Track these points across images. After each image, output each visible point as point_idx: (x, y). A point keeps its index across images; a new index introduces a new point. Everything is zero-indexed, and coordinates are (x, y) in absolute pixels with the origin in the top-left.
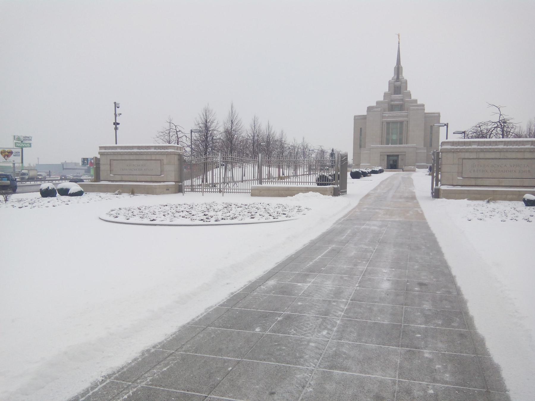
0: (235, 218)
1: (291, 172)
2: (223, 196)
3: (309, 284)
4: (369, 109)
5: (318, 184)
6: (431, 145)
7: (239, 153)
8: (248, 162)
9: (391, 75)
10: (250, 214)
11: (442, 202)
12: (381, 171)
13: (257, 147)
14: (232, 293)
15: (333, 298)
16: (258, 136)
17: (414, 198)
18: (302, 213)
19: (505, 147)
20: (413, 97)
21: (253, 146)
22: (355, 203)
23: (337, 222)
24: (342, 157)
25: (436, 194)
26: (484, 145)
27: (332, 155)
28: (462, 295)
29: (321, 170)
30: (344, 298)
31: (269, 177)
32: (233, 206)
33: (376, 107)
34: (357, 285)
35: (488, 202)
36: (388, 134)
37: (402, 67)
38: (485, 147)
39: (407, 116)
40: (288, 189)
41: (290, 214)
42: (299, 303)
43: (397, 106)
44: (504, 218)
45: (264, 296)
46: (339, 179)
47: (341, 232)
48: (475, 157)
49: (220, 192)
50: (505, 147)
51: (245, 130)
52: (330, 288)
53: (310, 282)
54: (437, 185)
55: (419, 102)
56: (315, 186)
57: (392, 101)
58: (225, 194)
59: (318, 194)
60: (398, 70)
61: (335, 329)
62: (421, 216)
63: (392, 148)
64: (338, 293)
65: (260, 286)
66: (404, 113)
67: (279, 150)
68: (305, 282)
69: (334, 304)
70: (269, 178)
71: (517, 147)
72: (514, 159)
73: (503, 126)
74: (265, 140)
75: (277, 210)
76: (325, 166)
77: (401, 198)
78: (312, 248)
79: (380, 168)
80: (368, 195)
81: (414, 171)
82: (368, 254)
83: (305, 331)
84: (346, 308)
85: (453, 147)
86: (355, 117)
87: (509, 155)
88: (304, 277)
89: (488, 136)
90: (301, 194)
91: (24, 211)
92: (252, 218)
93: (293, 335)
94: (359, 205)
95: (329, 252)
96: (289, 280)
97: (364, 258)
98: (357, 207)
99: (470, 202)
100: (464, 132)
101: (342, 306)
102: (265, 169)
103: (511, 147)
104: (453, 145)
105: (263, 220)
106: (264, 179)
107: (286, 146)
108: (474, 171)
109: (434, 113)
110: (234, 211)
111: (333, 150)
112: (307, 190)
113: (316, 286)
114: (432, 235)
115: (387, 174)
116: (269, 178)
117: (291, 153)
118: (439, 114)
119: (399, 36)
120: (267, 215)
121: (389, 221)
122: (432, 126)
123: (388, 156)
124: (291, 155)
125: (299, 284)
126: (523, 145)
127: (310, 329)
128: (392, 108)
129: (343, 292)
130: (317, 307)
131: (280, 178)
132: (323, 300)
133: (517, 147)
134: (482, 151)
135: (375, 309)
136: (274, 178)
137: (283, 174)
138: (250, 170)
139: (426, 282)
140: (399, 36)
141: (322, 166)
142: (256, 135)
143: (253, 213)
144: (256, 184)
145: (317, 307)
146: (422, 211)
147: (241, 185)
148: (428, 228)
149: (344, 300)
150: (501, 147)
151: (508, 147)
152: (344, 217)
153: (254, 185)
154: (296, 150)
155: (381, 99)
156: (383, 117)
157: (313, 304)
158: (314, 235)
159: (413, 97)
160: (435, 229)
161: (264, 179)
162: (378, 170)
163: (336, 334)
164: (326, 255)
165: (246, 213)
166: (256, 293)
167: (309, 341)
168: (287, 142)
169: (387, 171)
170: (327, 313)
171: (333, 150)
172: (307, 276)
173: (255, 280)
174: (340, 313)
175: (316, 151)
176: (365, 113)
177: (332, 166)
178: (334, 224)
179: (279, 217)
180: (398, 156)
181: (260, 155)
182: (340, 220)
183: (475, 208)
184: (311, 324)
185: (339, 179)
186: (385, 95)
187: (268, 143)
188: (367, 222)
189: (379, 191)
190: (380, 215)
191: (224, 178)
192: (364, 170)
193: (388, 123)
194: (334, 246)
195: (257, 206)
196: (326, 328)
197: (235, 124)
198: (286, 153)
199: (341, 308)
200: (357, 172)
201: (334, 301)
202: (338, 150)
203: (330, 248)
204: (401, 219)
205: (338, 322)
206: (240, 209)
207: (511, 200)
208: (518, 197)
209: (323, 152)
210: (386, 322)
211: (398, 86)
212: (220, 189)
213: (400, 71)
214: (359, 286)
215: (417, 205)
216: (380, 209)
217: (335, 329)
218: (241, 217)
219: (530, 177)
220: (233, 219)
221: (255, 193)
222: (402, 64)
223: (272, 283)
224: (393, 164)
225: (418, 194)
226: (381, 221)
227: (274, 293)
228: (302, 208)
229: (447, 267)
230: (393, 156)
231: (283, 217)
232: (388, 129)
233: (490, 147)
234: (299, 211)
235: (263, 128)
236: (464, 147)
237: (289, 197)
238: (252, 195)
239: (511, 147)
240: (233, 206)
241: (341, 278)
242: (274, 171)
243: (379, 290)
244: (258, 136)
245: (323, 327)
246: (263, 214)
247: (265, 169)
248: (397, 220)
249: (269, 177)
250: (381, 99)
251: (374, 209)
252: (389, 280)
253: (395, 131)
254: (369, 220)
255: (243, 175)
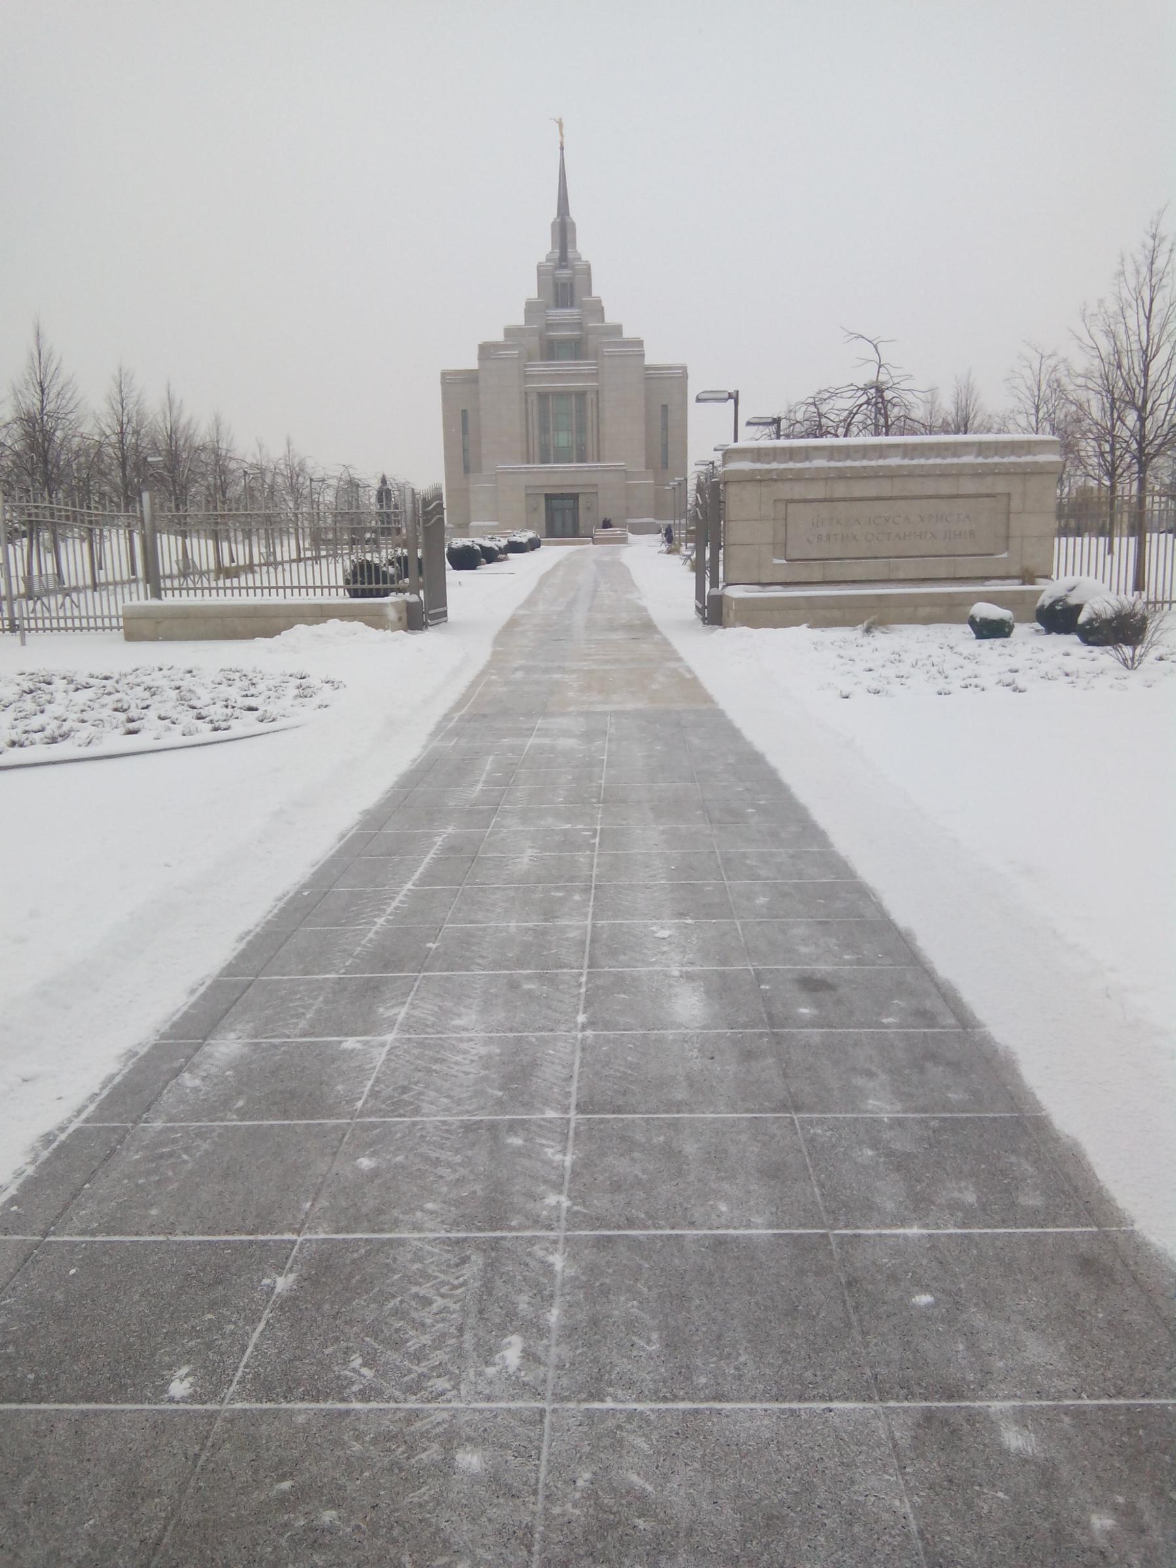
0: (65, 736)
1: (259, 551)
2: (23, 643)
3: (390, 1037)
4: (486, 351)
5: (354, 594)
6: (665, 465)
7: (69, 493)
8: (111, 521)
9: (543, 247)
10: (122, 716)
11: (735, 639)
12: (533, 545)
13: (136, 468)
14: (48, 1139)
15: (500, 1104)
16: (136, 432)
17: (648, 627)
18: (316, 700)
19: (906, 462)
20: (610, 318)
21: (123, 466)
22: (481, 653)
23: (439, 727)
24: (426, 503)
25: (714, 613)
26: (848, 457)
27: (384, 494)
28: (979, 1025)
29: (353, 542)
30: (546, 1102)
31: (187, 569)
32: (60, 684)
33: (504, 346)
34: (581, 1018)
35: (868, 631)
36: (544, 429)
37: (573, 224)
38: (849, 463)
39: (595, 375)
40: (255, 613)
41: (273, 709)
42: (365, 1163)
43: (564, 342)
44: (941, 684)
45: (201, 1134)
46: (421, 572)
47: (463, 768)
48: (821, 496)
49: (13, 628)
50: (906, 462)
51: (90, 414)
52: (483, 1051)
53: (391, 1023)
54: (715, 583)
55: (628, 333)
56: (342, 598)
57: (550, 326)
58: (30, 637)
59: (358, 625)
60: (563, 231)
61: (554, 1316)
62: (691, 686)
63: (562, 474)
64: (517, 1075)
65: (177, 1072)
66: (584, 366)
67: (210, 479)
68: (369, 1025)
69: (516, 1141)
70: (184, 574)
71: (939, 461)
72: (931, 497)
73: (878, 399)
74: (163, 446)
75: (225, 691)
76: (365, 530)
77: (613, 628)
78: (373, 847)
79: (530, 534)
80: (512, 624)
81: (623, 541)
82: (582, 857)
83: (419, 1356)
84: (568, 1160)
85: (759, 466)
86: (444, 374)
87: (916, 487)
88: (360, 1001)
89: (841, 431)
90: (301, 630)
91: (991, 336)
92: (130, 732)
93: (363, 1396)
94: (496, 662)
95: (437, 861)
96: (303, 1024)
97: (572, 879)
98: (490, 665)
99: (817, 632)
100: (777, 421)
101: (551, 1153)
102: (169, 547)
103: (922, 461)
104: (759, 460)
105: (174, 737)
106: (165, 577)
107: (232, 465)
108: (819, 537)
109: (670, 368)
110: (62, 701)
111: (384, 481)
112: (320, 614)
113: (421, 1044)
114: (757, 759)
115: (551, 554)
116: (184, 574)
117: (252, 489)
118: (684, 369)
119: (561, 125)
120: (188, 718)
121: (605, 713)
122: (665, 407)
123: (548, 497)
124: (252, 496)
125: (350, 1043)
126: (954, 455)
127: (439, 1341)
128: (551, 349)
129: (534, 1064)
130: (444, 1171)
131: (223, 572)
132: (468, 1128)
133: (939, 461)
134: (842, 476)
135: (690, 1148)
136: (202, 574)
137: (232, 561)
138: (117, 546)
139: (823, 968)
140: (561, 125)
141: (353, 531)
142: (129, 430)
143: (134, 713)
144: (139, 599)
145: (444, 1171)
146: (689, 670)
147: (91, 603)
148: (734, 734)
149: (551, 1114)
150: (894, 461)
151: (915, 462)
152: (459, 705)
153: (135, 602)
154: (268, 480)
155: (519, 320)
156: (527, 377)
157: (427, 1159)
158: (371, 788)
159: (610, 318)
160: (757, 735)
161: (165, 577)
162: (524, 540)
163: (565, 1351)
164: (429, 877)
165: (106, 713)
166: (158, 1124)
167: (451, 1439)
168: (238, 454)
169: (549, 544)
170: (495, 1209)
171: (384, 481)
172: (371, 991)
173: (153, 1039)
174: (552, 1199)
175: (334, 482)
176: (472, 363)
177: (386, 532)
178: (433, 735)
179: (232, 722)
180: (575, 497)
181: (146, 496)
182: (447, 717)
183: (842, 653)
184: (439, 1302)
185: (421, 572)
186: (531, 309)
187: (173, 456)
188: (540, 723)
189: (541, 608)
190: (571, 694)
191: (28, 580)
192: (487, 543)
193: (543, 396)
194: (450, 830)
195: (148, 681)
196: (510, 1320)
197: (52, 395)
198: (235, 491)
199: (548, 1163)
200: (467, 550)
201: (513, 1127)
202: (401, 480)
203: (439, 840)
204: (640, 705)
205: (558, 1261)
206: (83, 696)
207: (927, 621)
208: (948, 611)
209: (353, 486)
210: (760, 1231)
211: (564, 281)
212: (12, 620)
213: (569, 237)
214: (591, 1024)
215: (669, 653)
216: (561, 669)
217: (554, 1316)
218: (86, 731)
219: (974, 551)
220: (53, 740)
221: (140, 628)
222: (574, 213)
223: (228, 1046)
224: (563, 517)
225: (657, 614)
226: (581, 714)
227: (243, 1114)
228: (314, 681)
229: (863, 892)
230: (562, 496)
231: (245, 724)
232: (544, 413)
233: (865, 463)
234: (304, 692)
235: (152, 406)
236: (791, 465)
237: (261, 642)
238: (130, 637)
239: (922, 461)
240: (60, 684)
241: (514, 985)
242: (202, 550)
243: (670, 1034)
244: (136, 432)
245: (495, 1313)
246: (173, 714)
247: (169, 547)
248: (629, 706)
249: (187, 569)
250: (519, 320)
251: (547, 671)
252: (689, 977)
253: (561, 421)
254: (544, 714)
255: (96, 564)
